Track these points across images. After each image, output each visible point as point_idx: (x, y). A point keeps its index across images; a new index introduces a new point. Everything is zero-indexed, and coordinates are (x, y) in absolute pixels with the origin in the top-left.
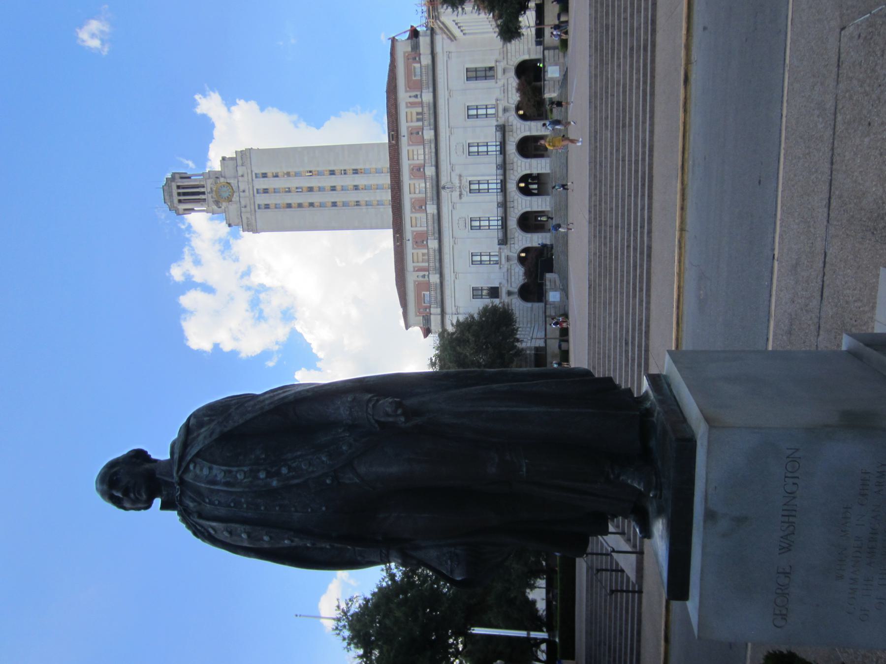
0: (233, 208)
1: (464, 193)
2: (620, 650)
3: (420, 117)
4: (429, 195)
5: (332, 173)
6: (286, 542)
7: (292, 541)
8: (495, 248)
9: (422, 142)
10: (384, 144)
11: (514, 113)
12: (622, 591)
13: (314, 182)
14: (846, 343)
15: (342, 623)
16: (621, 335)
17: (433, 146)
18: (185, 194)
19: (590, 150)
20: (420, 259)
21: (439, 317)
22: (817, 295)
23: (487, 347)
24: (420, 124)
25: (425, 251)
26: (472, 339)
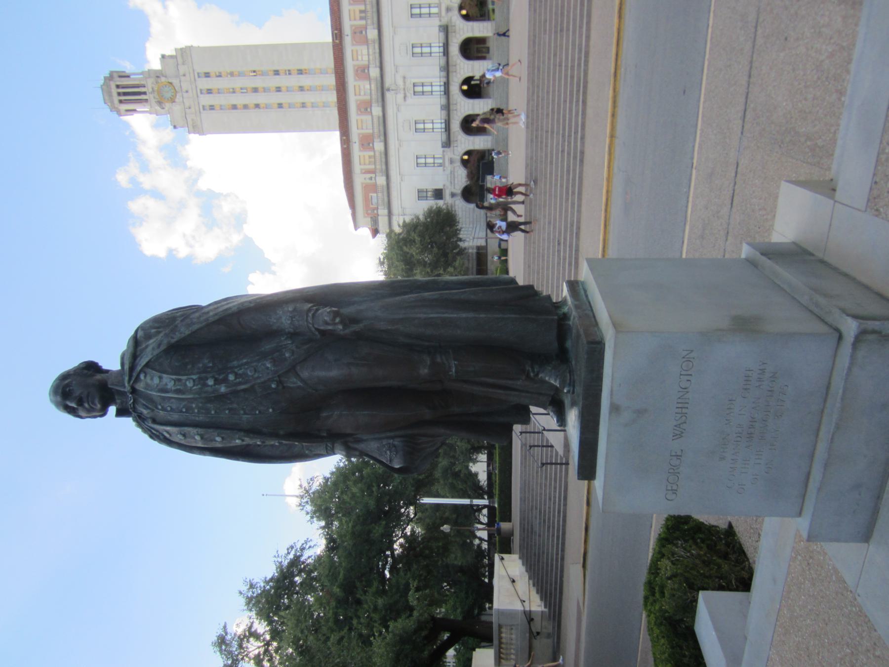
0: (177, 108)
1: (408, 94)
2: (550, 512)
3: (363, 15)
4: (374, 97)
5: (277, 73)
6: (237, 441)
7: (243, 441)
8: (438, 150)
9: (366, 41)
10: (322, 45)
11: (456, 12)
12: (551, 464)
13: (259, 82)
14: (745, 251)
15: (305, 500)
16: (554, 236)
17: (377, 46)
18: (125, 94)
19: (529, 54)
20: (367, 162)
21: (386, 218)
22: (728, 202)
23: (432, 247)
24: (363, 22)
25: (372, 153)
26: (418, 239)
